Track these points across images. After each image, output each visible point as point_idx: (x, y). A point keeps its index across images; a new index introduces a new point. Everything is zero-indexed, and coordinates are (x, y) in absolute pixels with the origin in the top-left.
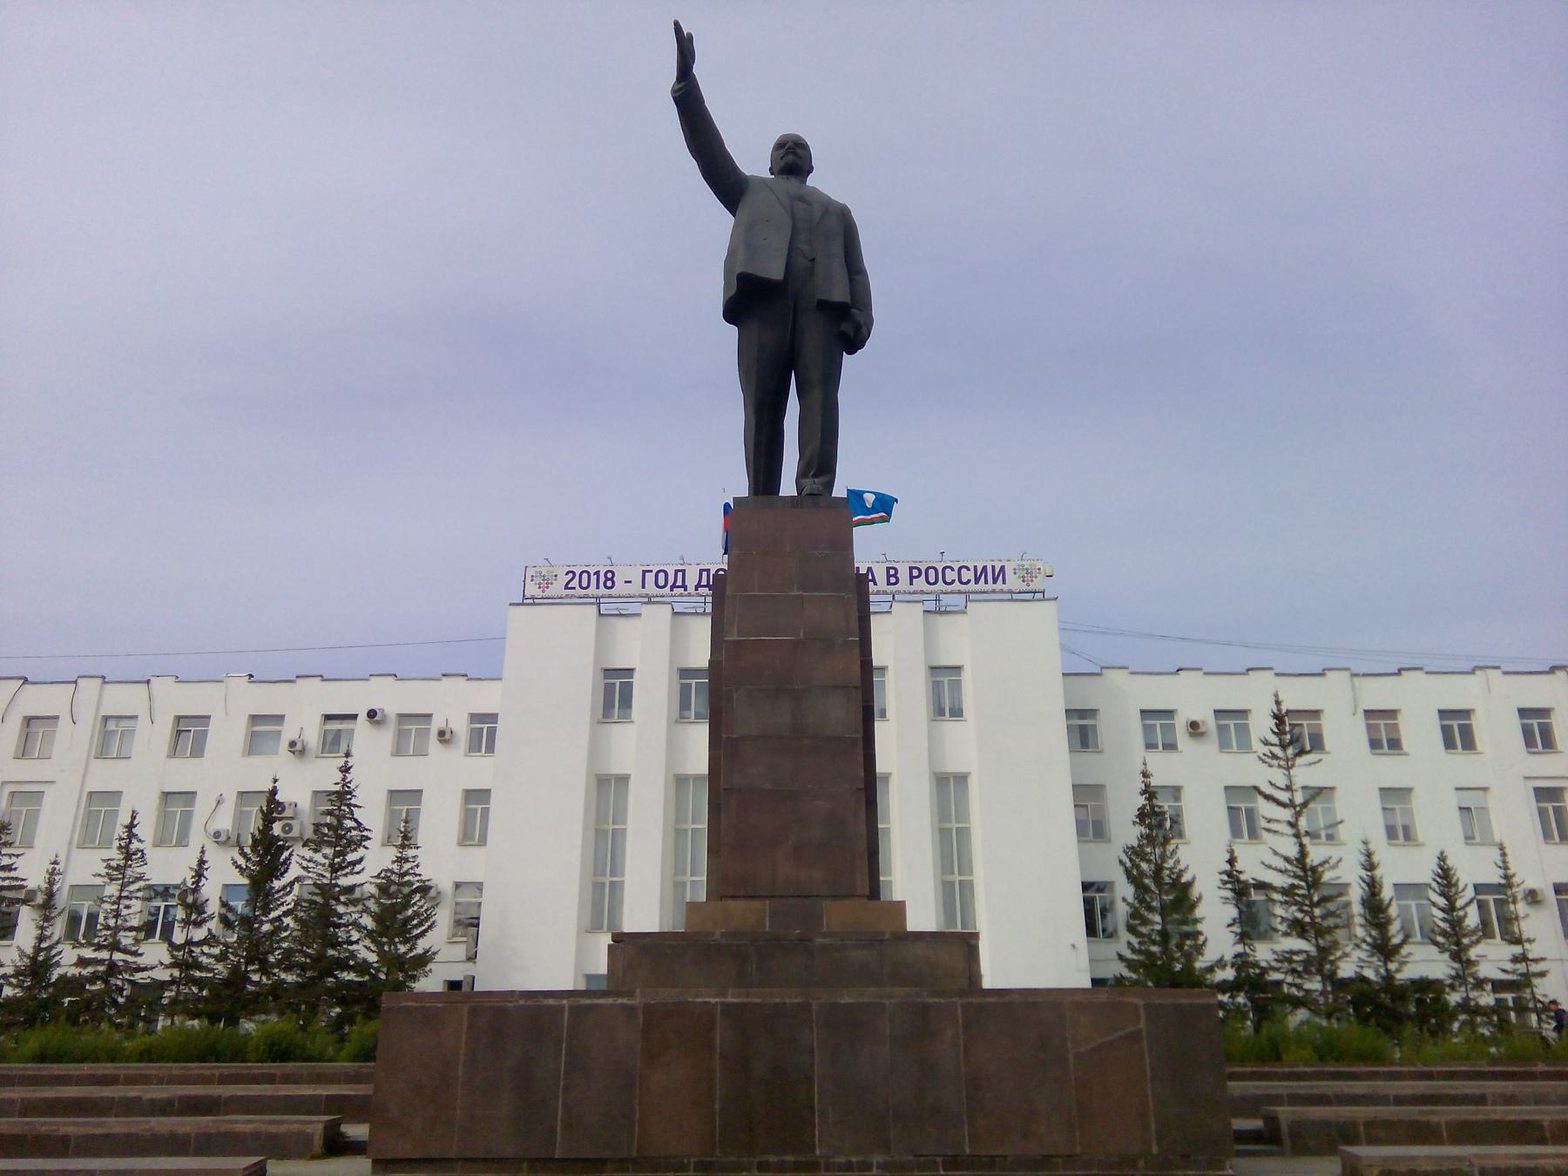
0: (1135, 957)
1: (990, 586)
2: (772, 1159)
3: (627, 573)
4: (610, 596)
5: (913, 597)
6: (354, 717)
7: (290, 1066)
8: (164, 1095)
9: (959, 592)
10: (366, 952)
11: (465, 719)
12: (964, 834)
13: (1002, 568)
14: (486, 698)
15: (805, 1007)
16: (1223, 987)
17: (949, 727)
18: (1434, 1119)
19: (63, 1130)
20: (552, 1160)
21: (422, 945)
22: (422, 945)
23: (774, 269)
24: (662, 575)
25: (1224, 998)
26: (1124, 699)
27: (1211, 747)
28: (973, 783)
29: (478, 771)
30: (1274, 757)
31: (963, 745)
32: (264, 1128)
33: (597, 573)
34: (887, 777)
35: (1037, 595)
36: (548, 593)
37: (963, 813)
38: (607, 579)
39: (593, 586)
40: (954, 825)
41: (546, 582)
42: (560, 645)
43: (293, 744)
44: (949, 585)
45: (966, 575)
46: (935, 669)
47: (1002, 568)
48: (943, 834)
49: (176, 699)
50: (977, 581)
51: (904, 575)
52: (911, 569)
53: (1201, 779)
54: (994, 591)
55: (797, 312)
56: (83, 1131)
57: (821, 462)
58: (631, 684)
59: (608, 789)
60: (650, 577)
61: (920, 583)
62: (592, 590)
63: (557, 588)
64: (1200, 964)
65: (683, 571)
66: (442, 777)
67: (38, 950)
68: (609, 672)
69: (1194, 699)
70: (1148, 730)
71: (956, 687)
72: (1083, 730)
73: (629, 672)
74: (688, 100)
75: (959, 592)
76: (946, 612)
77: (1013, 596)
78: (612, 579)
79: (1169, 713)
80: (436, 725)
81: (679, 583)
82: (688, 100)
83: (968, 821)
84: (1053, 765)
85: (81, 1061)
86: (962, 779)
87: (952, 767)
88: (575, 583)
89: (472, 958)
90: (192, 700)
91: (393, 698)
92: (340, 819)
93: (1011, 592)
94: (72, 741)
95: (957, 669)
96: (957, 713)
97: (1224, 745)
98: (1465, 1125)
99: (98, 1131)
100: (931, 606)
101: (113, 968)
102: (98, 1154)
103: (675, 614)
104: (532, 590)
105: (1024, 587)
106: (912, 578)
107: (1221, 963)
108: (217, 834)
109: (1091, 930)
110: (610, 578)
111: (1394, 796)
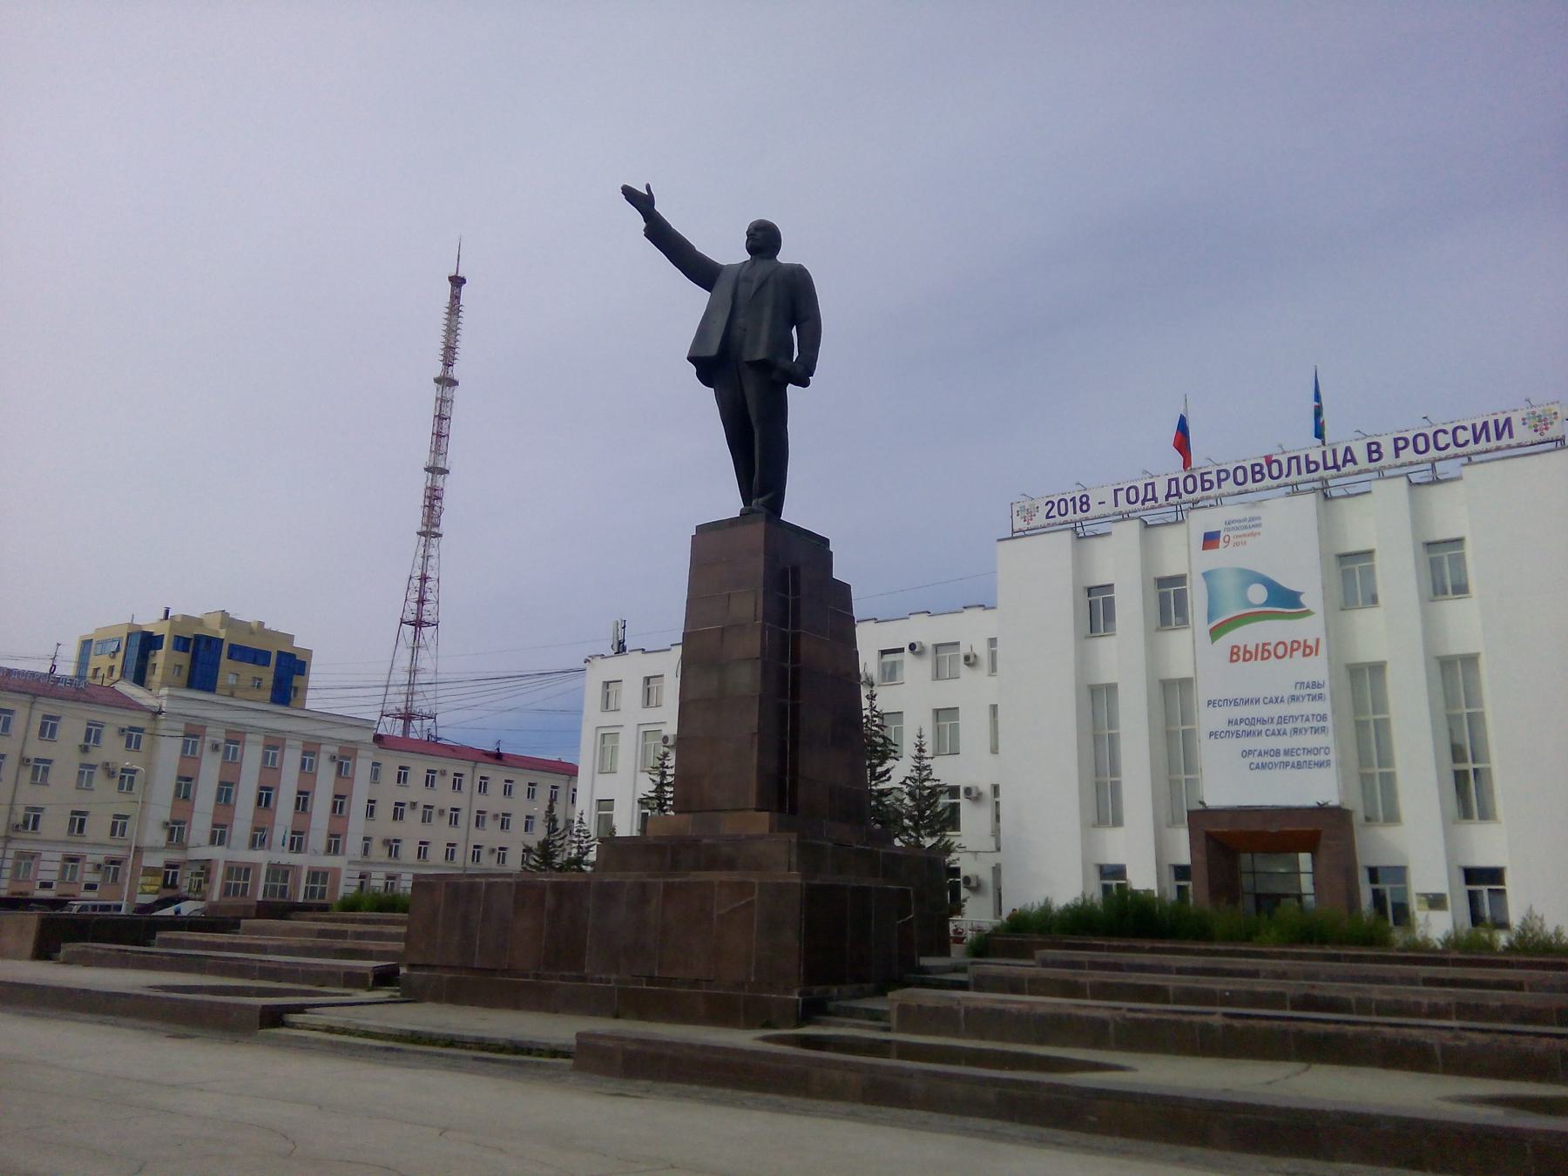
1: (1494, 443)
3: (1100, 497)
6: (902, 650)
9: (1456, 456)
12: (1383, 727)
13: (1508, 421)
18: (1081, 980)
24: (1132, 492)
28: (1483, 662)
31: (1464, 623)
33: (1073, 499)
36: (1033, 524)
39: (1073, 516)
40: (1371, 717)
41: (1029, 514)
42: (1041, 575)
47: (1508, 421)
50: (1476, 440)
51: (1387, 448)
52: (1396, 440)
54: (1498, 449)
58: (1112, 599)
59: (1098, 699)
60: (1122, 496)
61: (1408, 455)
62: (1070, 516)
63: (1039, 519)
65: (1153, 484)
68: (1162, 582)
73: (1109, 588)
74: (660, 234)
75: (1456, 456)
80: (964, 650)
82: (660, 234)
87: (1456, 648)
88: (1054, 512)
91: (926, 631)
93: (1520, 446)
96: (1461, 589)
98: (1105, 985)
103: (1147, 526)
104: (1019, 524)
105: (1537, 437)
106: (1397, 450)
110: (1085, 502)
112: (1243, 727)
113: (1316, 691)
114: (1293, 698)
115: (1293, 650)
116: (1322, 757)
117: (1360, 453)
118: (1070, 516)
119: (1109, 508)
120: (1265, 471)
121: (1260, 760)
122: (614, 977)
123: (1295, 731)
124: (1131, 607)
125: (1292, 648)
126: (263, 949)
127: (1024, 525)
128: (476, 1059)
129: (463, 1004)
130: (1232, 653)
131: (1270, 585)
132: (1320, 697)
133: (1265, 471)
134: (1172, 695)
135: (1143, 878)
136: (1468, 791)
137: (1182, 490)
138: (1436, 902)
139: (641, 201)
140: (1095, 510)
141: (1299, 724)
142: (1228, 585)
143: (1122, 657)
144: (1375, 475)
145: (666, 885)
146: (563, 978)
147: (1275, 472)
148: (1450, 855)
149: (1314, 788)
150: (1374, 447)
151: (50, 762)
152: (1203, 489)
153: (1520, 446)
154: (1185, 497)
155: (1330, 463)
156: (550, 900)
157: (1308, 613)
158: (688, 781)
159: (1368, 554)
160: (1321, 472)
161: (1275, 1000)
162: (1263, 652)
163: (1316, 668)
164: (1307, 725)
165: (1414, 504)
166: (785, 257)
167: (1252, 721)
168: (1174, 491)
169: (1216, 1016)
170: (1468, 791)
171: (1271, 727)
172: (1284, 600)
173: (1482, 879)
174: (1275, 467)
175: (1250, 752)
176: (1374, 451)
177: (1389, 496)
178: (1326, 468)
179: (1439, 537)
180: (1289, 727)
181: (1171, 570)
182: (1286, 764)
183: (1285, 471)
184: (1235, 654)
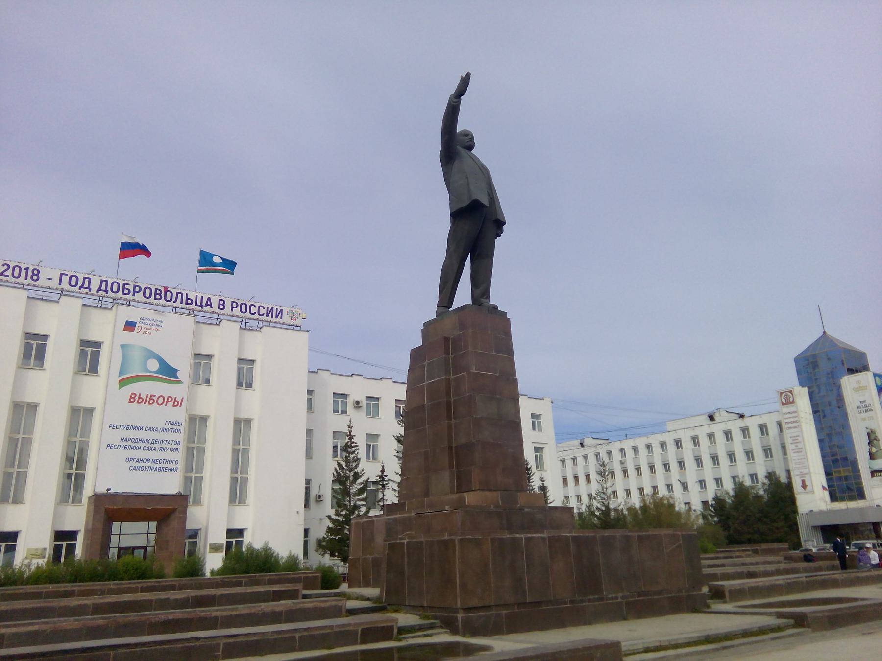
0: (337, 518)
1: (274, 319)
2: (591, 597)
3: (49, 275)
4: (35, 286)
5: (233, 318)
7: (145, 583)
8: (183, 596)
13: (281, 310)
15: (595, 537)
17: (245, 393)
19: (214, 614)
20: (525, 603)
22: (625, 512)
24: (74, 279)
27: (362, 413)
31: (252, 404)
32: (319, 605)
33: (27, 269)
35: (294, 327)
37: (247, 441)
38: (33, 274)
47: (281, 310)
48: (236, 452)
50: (267, 315)
51: (228, 305)
52: (233, 302)
54: (275, 322)
56: (225, 613)
58: (45, 345)
60: (65, 279)
61: (237, 311)
62: (22, 279)
69: (357, 390)
70: (335, 403)
71: (251, 371)
73: (45, 337)
75: (257, 320)
76: (249, 330)
78: (37, 275)
79: (346, 396)
81: (86, 285)
83: (32, 433)
85: (59, 582)
86: (248, 422)
87: (244, 415)
88: (9, 272)
93: (284, 324)
95: (252, 362)
96: (250, 385)
97: (368, 413)
99: (234, 613)
105: (291, 322)
106: (233, 307)
110: (36, 274)
112: (130, 443)
113: (177, 427)
114: (163, 430)
115: (168, 402)
116: (174, 466)
117: (215, 303)
120: (163, 295)
121: (137, 464)
122: (620, 595)
123: (161, 449)
125: (168, 400)
128: (773, 639)
129: (266, 654)
130: (131, 397)
131: (161, 361)
132: (179, 431)
133: (163, 295)
134: (80, 416)
137: (109, 289)
138: (215, 548)
141: (164, 445)
142: (136, 356)
144: (187, 312)
145: (639, 536)
146: (589, 601)
147: (168, 298)
149: (169, 484)
150: (36, 272)
151: (377, 399)
152: (123, 293)
153: (284, 324)
154: (110, 294)
155: (199, 303)
156: (572, 548)
157: (180, 382)
160: (193, 306)
162: (151, 400)
163: (180, 415)
164: (168, 446)
165: (241, 336)
167: (136, 441)
168: (103, 288)
171: (147, 445)
172: (168, 372)
173: (235, 533)
174: (169, 294)
175: (131, 459)
176: (222, 304)
177: (230, 328)
178: (196, 305)
179: (203, 352)
180: (157, 446)
181: (93, 337)
182: (152, 468)
183: (174, 299)
184: (133, 398)
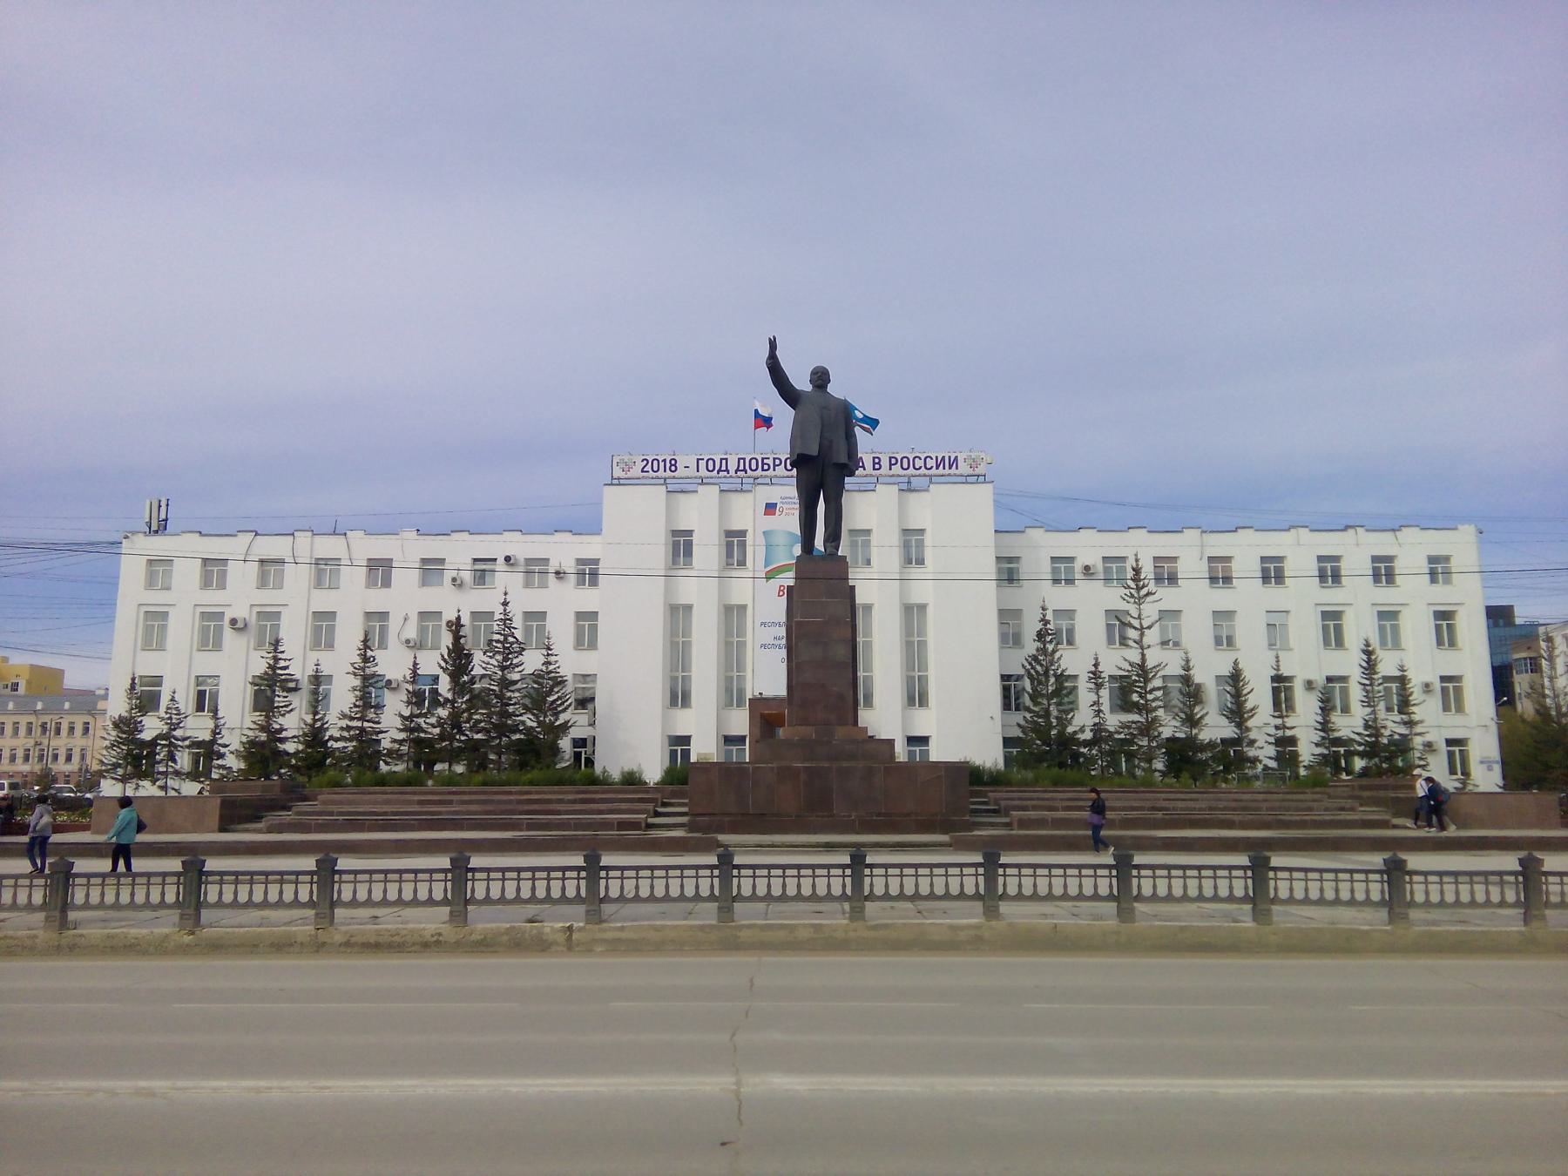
1: (947, 471)
3: (686, 461)
5: (892, 480)
10: (529, 720)
11: (573, 563)
12: (923, 645)
14: (589, 547)
16: (1086, 743)
21: (563, 718)
23: (813, 450)
25: (1085, 750)
26: (1040, 548)
28: (930, 611)
29: (588, 599)
30: (1132, 596)
34: (868, 608)
35: (980, 479)
36: (629, 475)
41: (627, 467)
43: (454, 580)
44: (915, 474)
45: (930, 463)
46: (906, 532)
48: (909, 645)
49: (367, 547)
51: (885, 463)
53: (1090, 604)
55: (825, 460)
57: (833, 536)
59: (678, 614)
60: (702, 464)
61: (897, 469)
62: (661, 473)
63: (636, 471)
64: (1070, 729)
66: (560, 604)
67: (315, 721)
68: (675, 533)
69: (1088, 548)
72: (1009, 573)
73: (690, 533)
77: (966, 480)
79: (1071, 559)
84: (986, 599)
88: (648, 468)
89: (592, 724)
90: (380, 547)
91: (523, 547)
92: (506, 637)
94: (297, 578)
100: (905, 486)
101: (362, 730)
102: (462, 829)
104: (618, 472)
105: (971, 471)
107: (1082, 730)
108: (408, 641)
109: (1006, 706)
110: (674, 464)
111: (1223, 617)
118: (661, 473)
119: (692, 472)
124: (707, 552)
126: (559, 813)
127: (623, 475)
135: (705, 748)
136: (916, 696)
139: (773, 344)
140: (681, 472)
143: (698, 588)
148: (904, 729)
158: (1211, 745)
159: (868, 532)
161: (1142, 809)
166: (831, 389)
169: (1160, 815)
170: (916, 696)
